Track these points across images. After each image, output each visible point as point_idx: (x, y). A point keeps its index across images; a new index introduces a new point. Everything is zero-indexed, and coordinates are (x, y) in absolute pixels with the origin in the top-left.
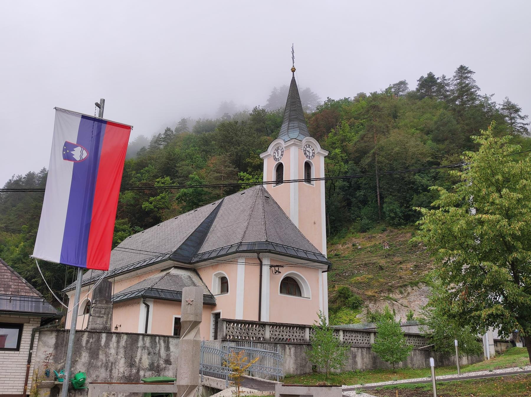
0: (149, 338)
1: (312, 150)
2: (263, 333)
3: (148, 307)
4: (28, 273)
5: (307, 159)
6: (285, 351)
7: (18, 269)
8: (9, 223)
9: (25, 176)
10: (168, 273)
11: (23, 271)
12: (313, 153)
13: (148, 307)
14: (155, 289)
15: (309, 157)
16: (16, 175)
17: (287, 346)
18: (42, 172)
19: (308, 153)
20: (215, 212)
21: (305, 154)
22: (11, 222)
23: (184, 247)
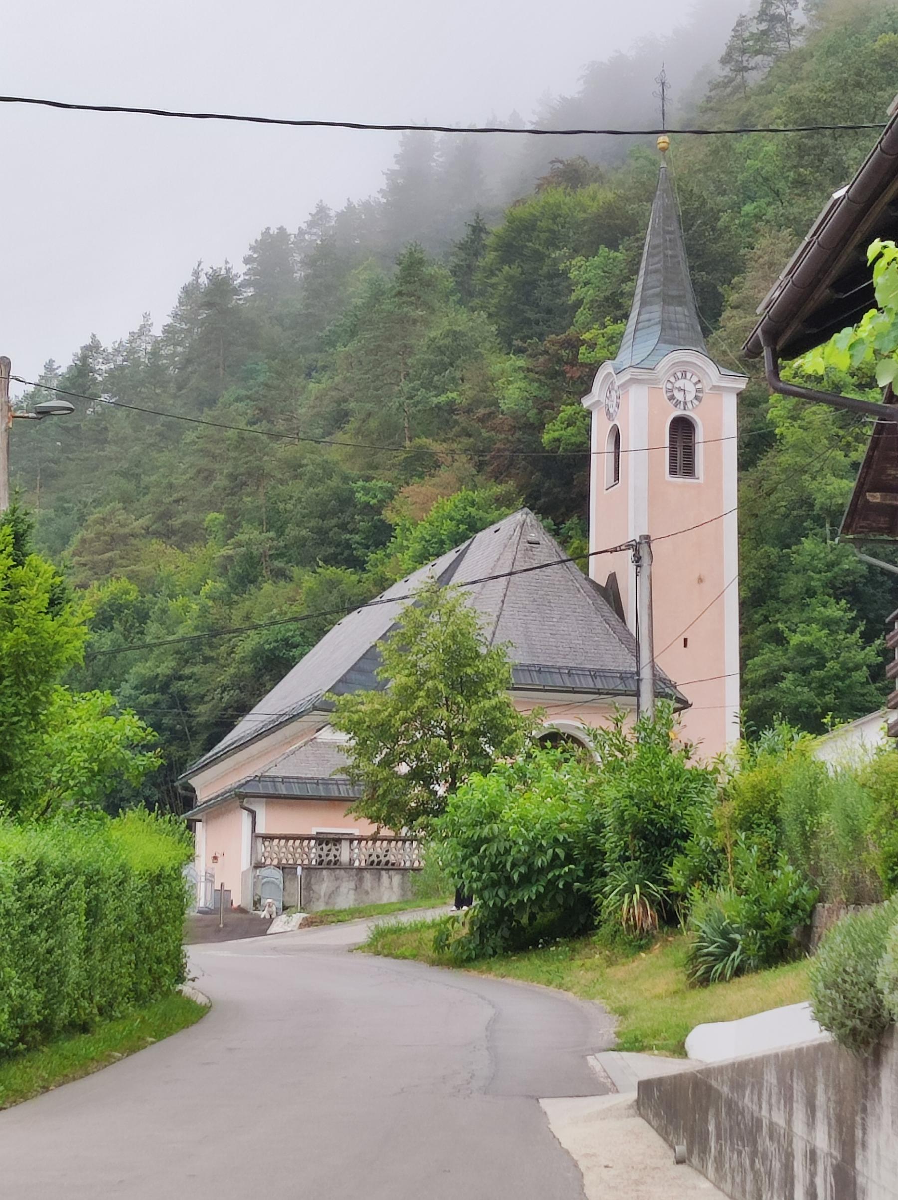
0: (396, 879)
1: (696, 384)
2: (337, 854)
3: (253, 814)
4: (226, 697)
5: (678, 412)
6: (379, 880)
7: (196, 681)
8: (169, 503)
9: (251, 253)
10: (312, 740)
11: (209, 687)
12: (698, 390)
13: (253, 814)
14: (269, 777)
15: (685, 403)
16: (206, 268)
17: (383, 873)
18: (311, 224)
19: (679, 396)
20: (446, 576)
21: (672, 398)
22: (175, 496)
23: (354, 676)
